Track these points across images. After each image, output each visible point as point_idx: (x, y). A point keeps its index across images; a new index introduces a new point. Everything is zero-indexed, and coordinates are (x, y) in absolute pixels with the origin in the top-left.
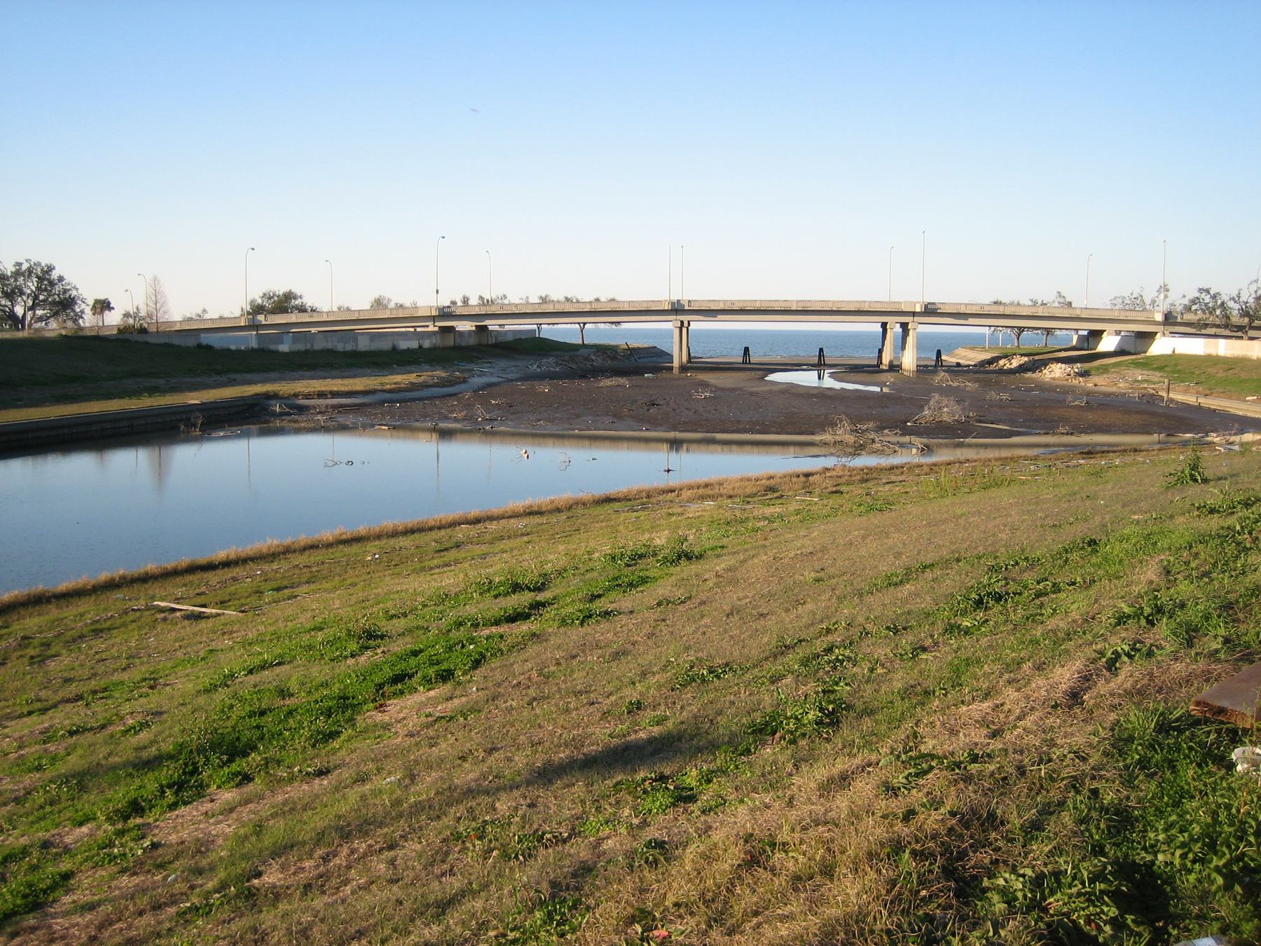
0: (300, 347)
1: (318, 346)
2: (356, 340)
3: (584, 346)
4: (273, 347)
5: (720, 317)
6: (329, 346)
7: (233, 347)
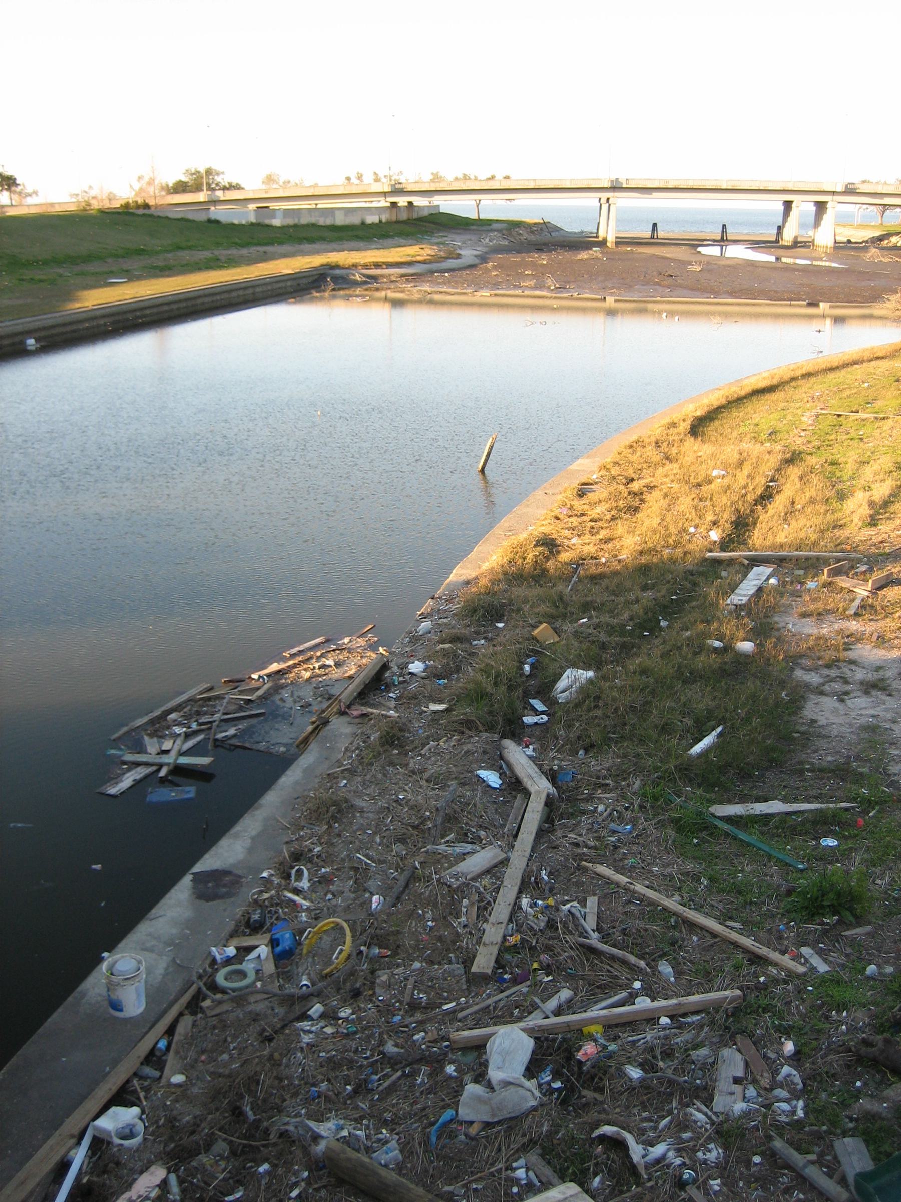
0: (290, 222)
1: (304, 221)
2: (334, 216)
3: (479, 220)
4: (267, 222)
5: (655, 195)
6: (313, 220)
7: (236, 222)
